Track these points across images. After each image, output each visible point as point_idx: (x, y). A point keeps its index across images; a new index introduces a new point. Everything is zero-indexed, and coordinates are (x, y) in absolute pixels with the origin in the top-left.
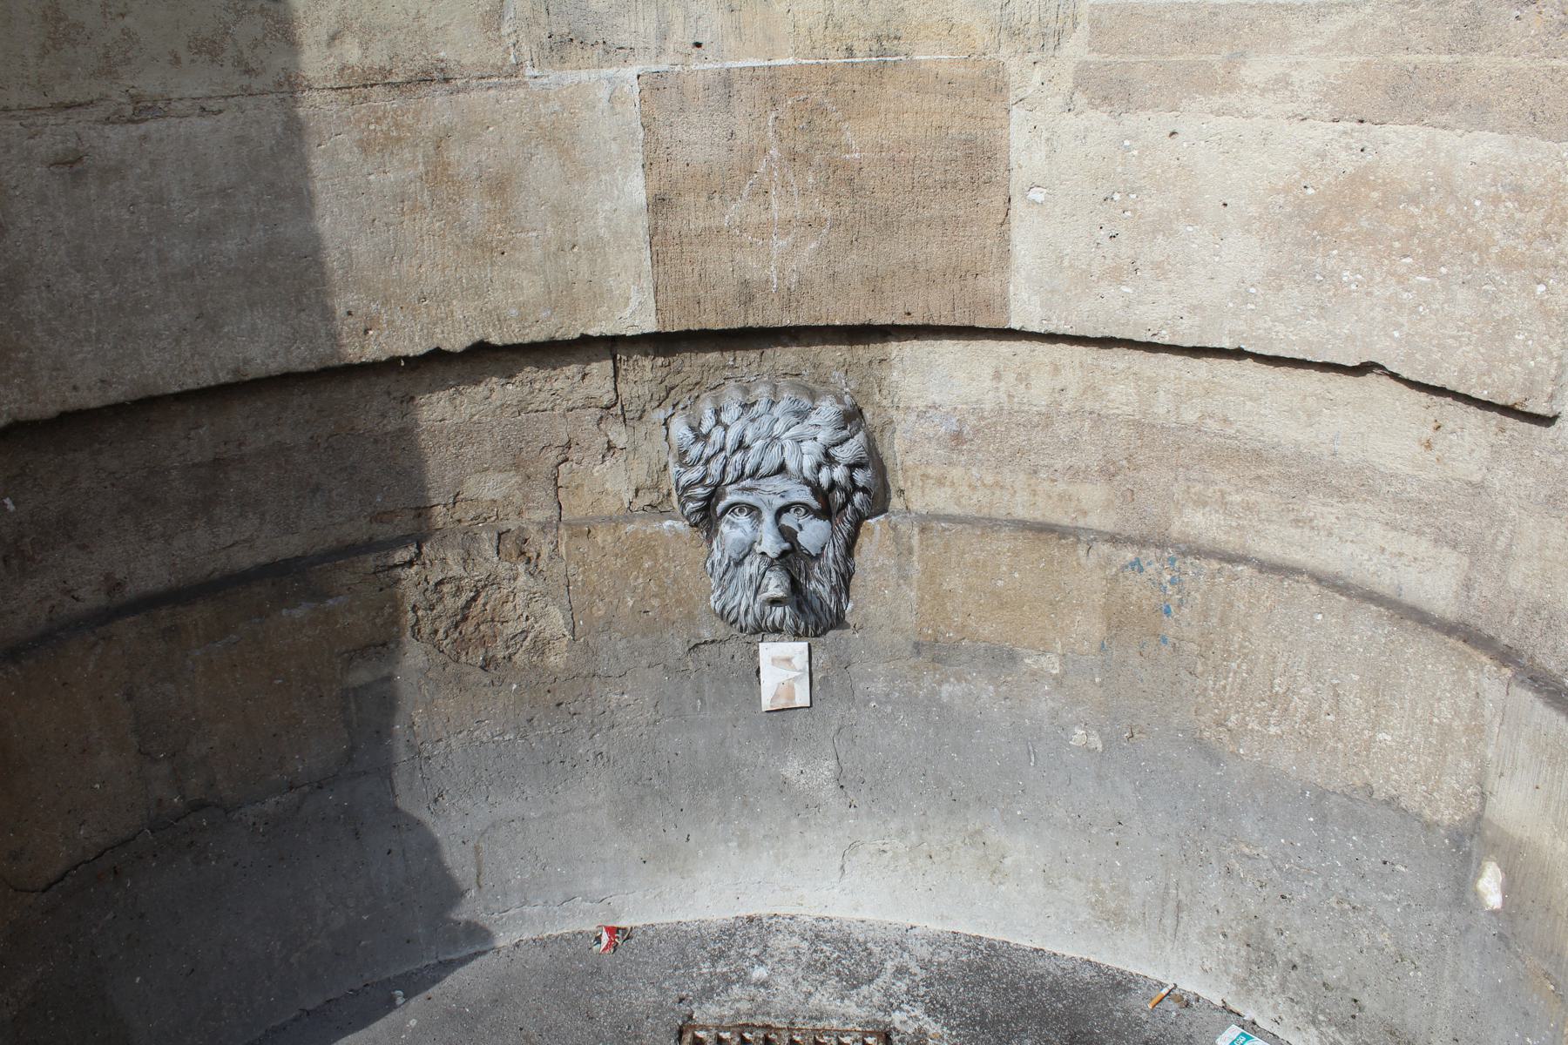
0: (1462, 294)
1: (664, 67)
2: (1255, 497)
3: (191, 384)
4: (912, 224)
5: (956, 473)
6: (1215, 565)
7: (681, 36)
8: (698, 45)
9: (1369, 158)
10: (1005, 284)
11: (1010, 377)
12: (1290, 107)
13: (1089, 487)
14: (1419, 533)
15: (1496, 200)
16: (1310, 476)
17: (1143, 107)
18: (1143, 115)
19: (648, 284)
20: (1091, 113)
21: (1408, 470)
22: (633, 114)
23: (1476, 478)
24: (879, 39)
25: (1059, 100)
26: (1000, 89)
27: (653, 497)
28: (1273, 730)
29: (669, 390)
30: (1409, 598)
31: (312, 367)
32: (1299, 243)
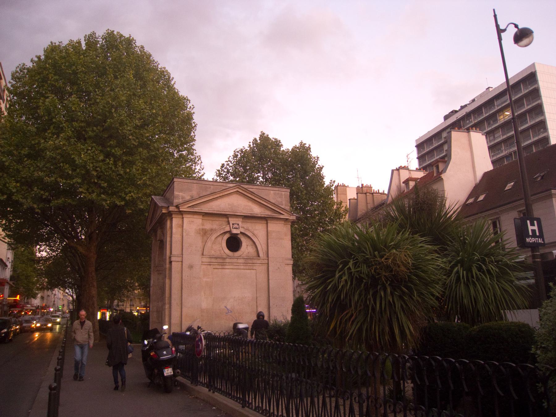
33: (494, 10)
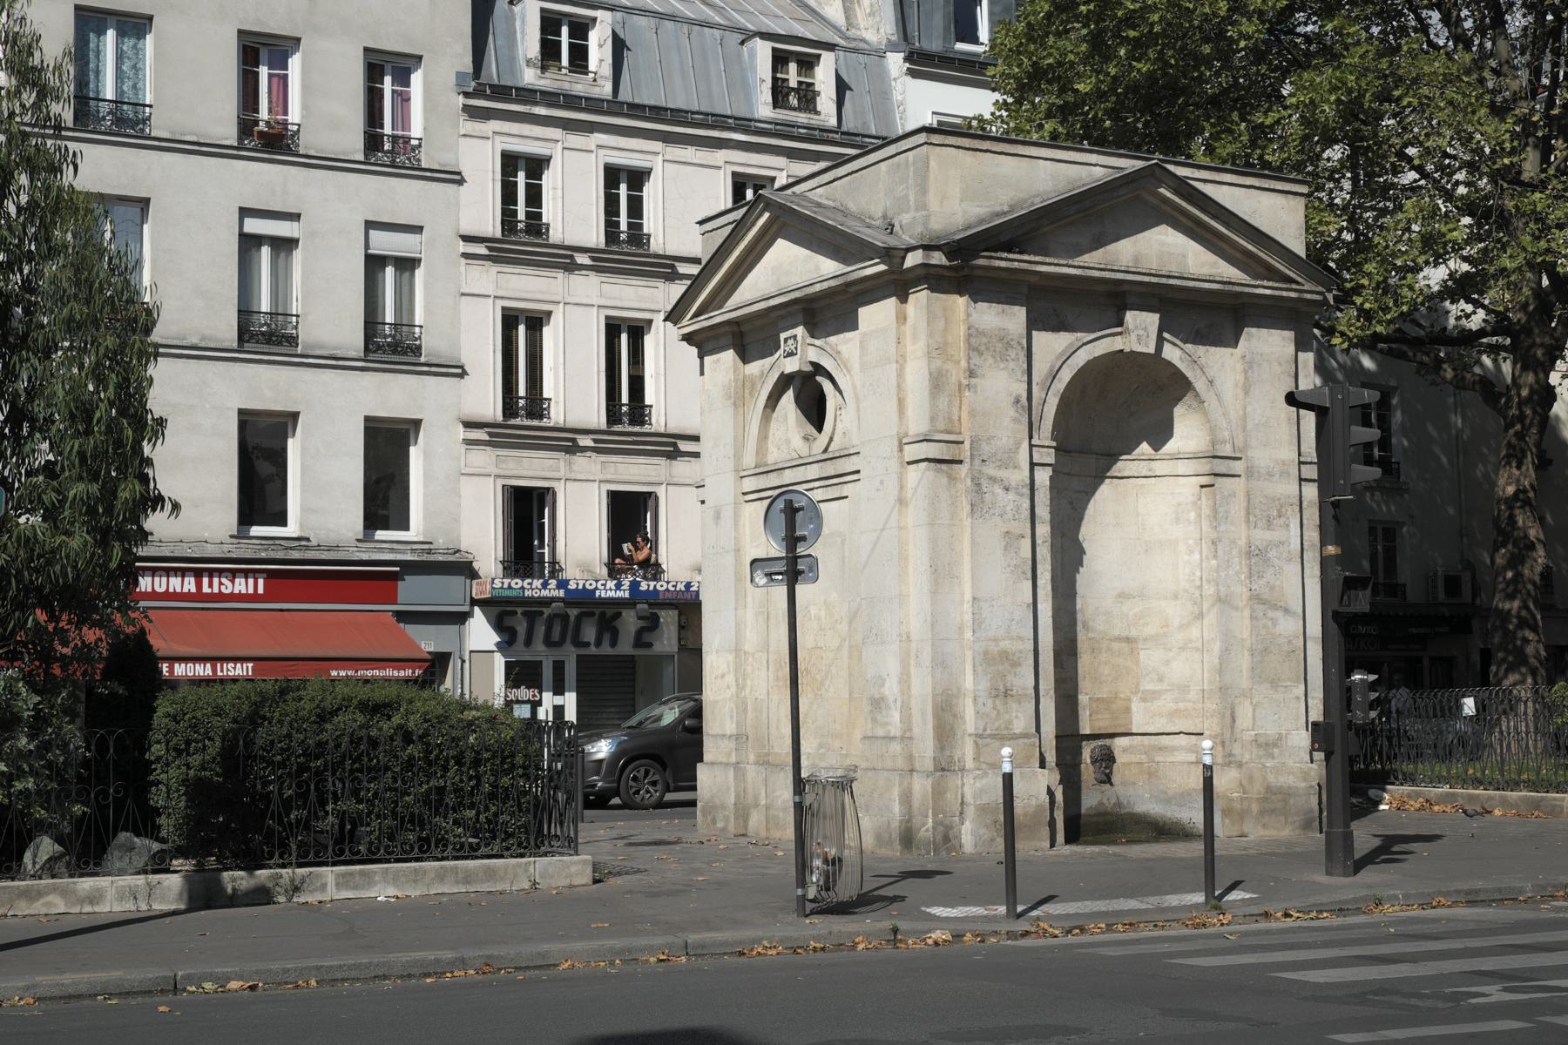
16: (1173, 749)
33: (702, 373)
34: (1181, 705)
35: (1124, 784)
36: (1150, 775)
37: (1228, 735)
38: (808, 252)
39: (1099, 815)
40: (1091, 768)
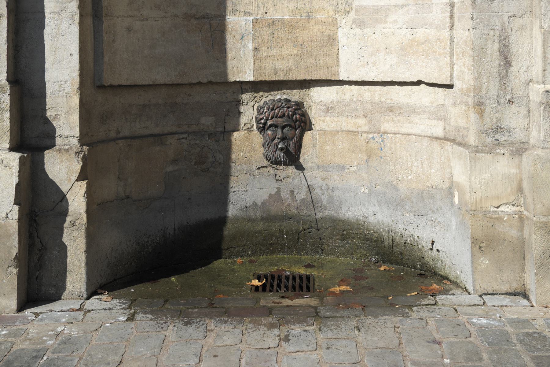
0: (434, 62)
1: (258, 18)
2: (399, 118)
3: (144, 83)
4: (316, 55)
5: (328, 118)
6: (392, 135)
7: (263, 10)
8: (266, 13)
9: (414, 36)
10: (338, 69)
11: (340, 93)
12: (398, 26)
13: (360, 119)
14: (435, 119)
15: (437, 42)
16: (409, 111)
17: (367, 27)
18: (368, 29)
19: (252, 68)
20: (356, 29)
21: (431, 105)
22: (251, 28)
23: (443, 103)
24: (308, 13)
25: (349, 26)
26: (336, 24)
27: (249, 126)
28: (410, 177)
29: (255, 97)
30: (435, 135)
31: (170, 83)
32: (402, 55)
34: (420, 33)
35: (324, 167)
36: (370, 154)
37: (494, 91)
38: (78, 124)
39: (269, 219)
40: (257, 138)
